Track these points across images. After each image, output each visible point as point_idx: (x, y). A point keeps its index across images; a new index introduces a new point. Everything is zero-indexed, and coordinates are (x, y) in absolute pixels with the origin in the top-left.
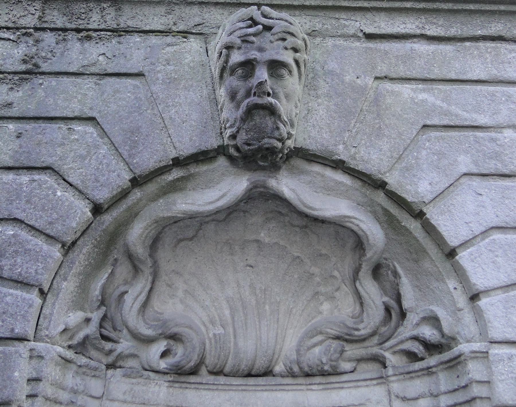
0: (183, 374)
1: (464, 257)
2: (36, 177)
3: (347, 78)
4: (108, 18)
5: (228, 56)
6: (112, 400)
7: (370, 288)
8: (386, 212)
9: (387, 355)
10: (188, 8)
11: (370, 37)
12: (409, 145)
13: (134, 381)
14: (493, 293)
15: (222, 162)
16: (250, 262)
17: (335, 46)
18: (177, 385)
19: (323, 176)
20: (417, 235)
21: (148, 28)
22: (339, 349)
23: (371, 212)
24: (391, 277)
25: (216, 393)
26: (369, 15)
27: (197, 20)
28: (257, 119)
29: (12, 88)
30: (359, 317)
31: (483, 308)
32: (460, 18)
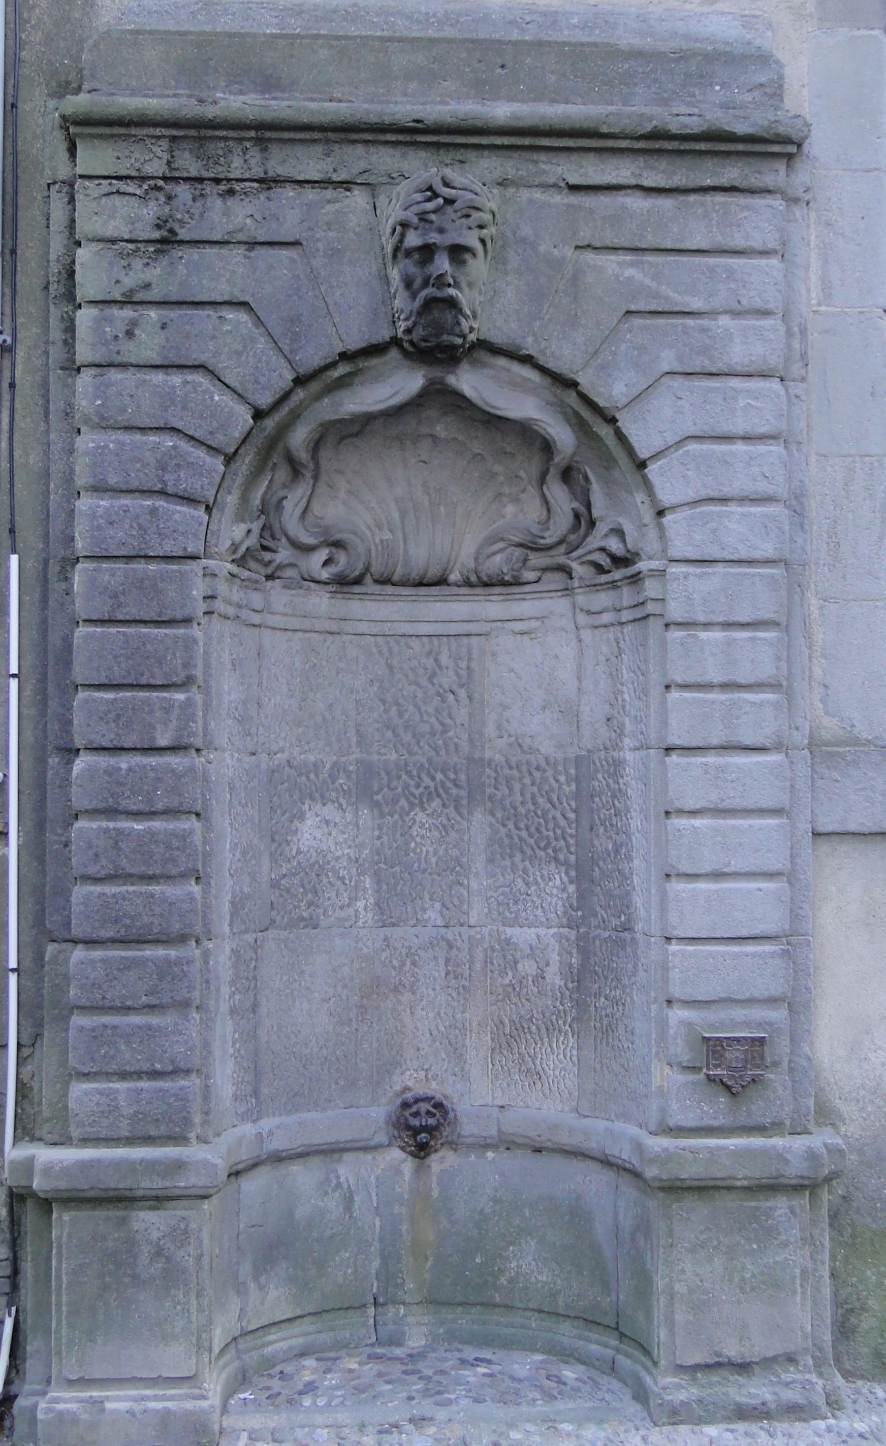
0: (345, 583)
1: (652, 470)
2: (190, 378)
3: (542, 248)
4: (253, 162)
5: (403, 236)
6: (272, 613)
7: (558, 493)
8: (577, 414)
9: (574, 565)
10: (351, 147)
11: (574, 188)
12: (607, 337)
13: (294, 592)
14: (679, 509)
15: (394, 354)
16: (424, 457)
17: (531, 201)
18: (339, 596)
19: (509, 371)
20: (608, 442)
21: (301, 178)
22: (522, 558)
23: (561, 413)
24: (582, 482)
25: (384, 603)
26: (575, 157)
27: (363, 165)
28: (436, 313)
29: (148, 264)
30: (545, 524)
31: (666, 526)
32: (688, 161)
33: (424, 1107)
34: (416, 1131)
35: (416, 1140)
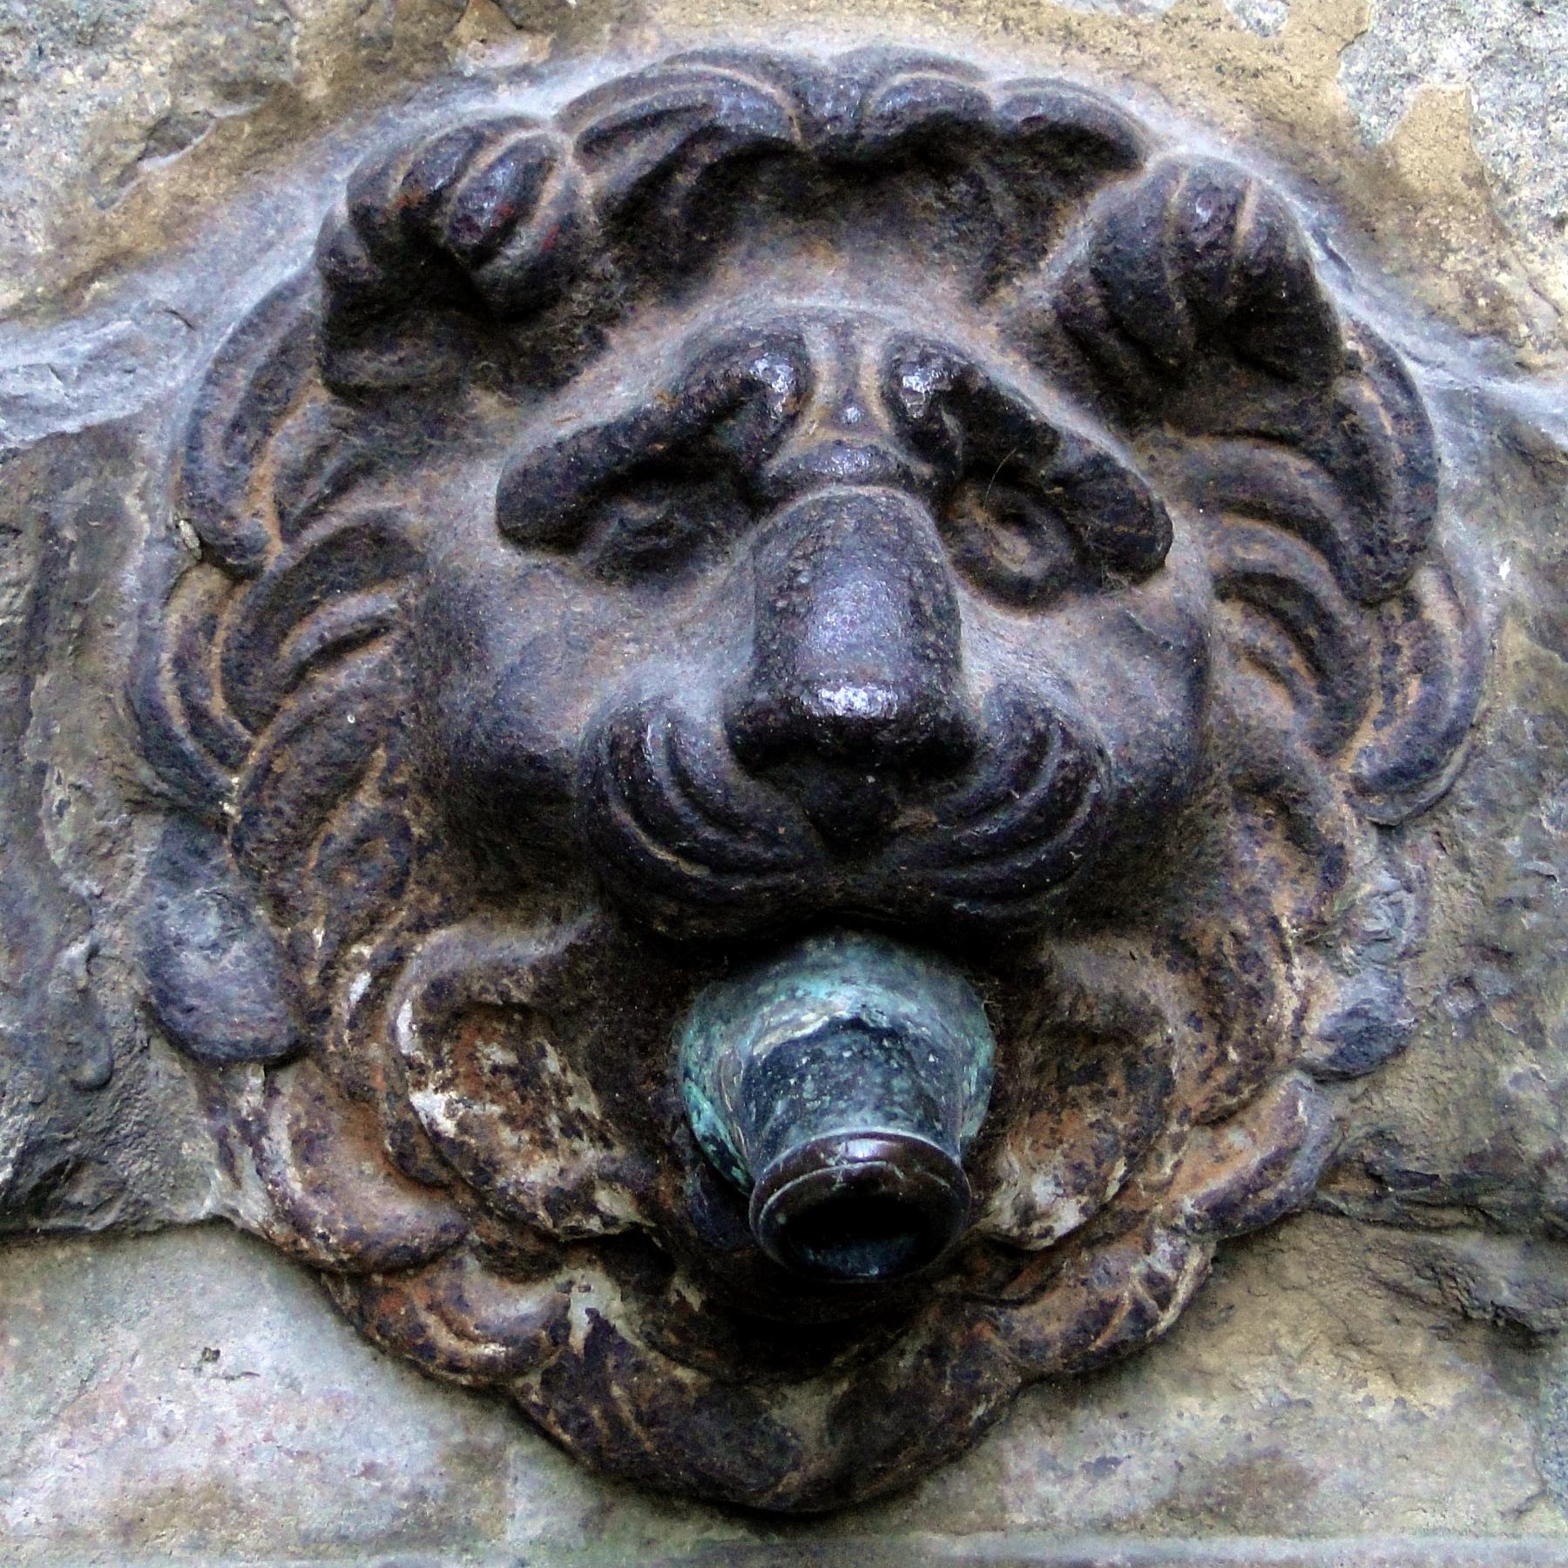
33: (850, 321)
34: (649, 895)
35: (644, 1117)
